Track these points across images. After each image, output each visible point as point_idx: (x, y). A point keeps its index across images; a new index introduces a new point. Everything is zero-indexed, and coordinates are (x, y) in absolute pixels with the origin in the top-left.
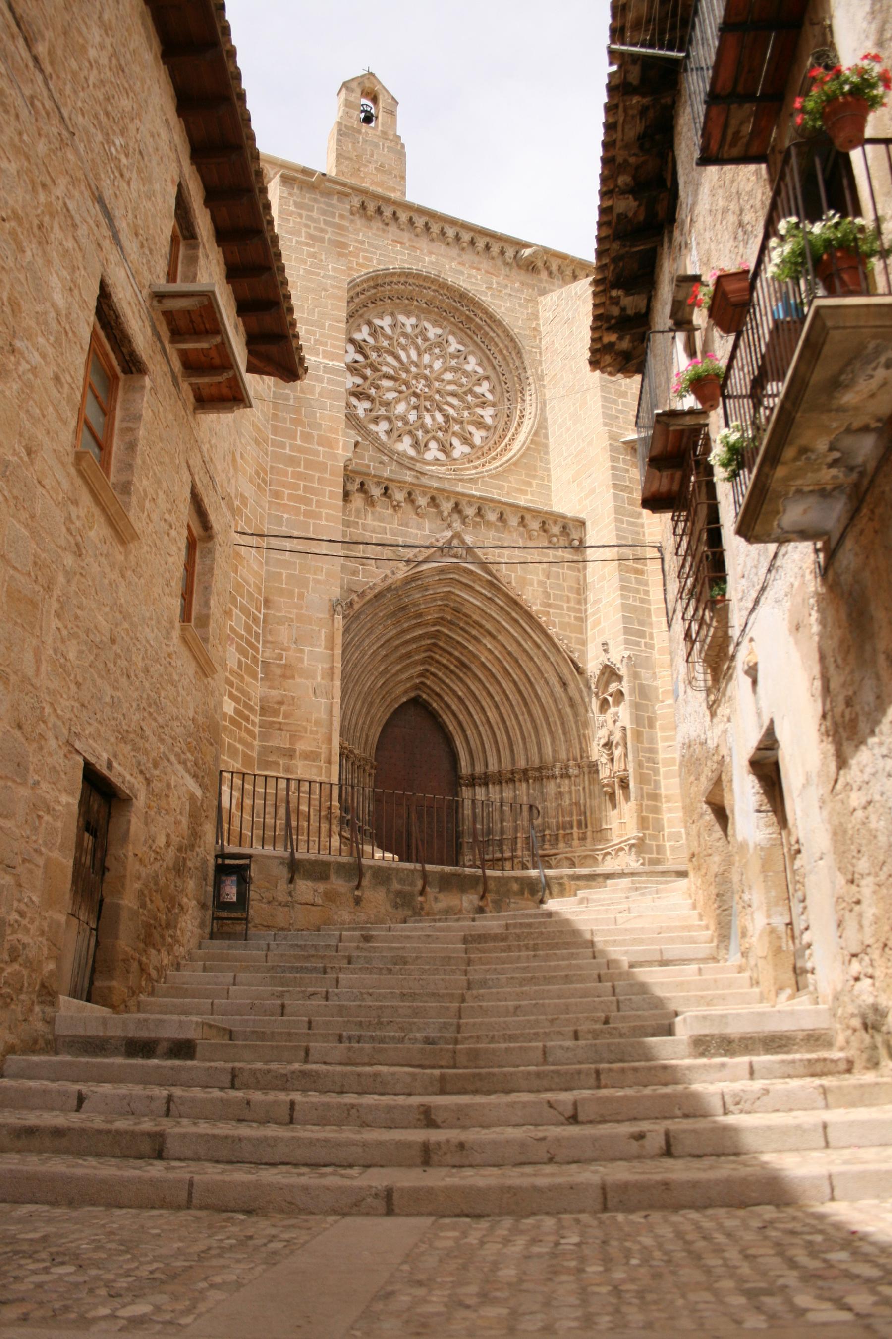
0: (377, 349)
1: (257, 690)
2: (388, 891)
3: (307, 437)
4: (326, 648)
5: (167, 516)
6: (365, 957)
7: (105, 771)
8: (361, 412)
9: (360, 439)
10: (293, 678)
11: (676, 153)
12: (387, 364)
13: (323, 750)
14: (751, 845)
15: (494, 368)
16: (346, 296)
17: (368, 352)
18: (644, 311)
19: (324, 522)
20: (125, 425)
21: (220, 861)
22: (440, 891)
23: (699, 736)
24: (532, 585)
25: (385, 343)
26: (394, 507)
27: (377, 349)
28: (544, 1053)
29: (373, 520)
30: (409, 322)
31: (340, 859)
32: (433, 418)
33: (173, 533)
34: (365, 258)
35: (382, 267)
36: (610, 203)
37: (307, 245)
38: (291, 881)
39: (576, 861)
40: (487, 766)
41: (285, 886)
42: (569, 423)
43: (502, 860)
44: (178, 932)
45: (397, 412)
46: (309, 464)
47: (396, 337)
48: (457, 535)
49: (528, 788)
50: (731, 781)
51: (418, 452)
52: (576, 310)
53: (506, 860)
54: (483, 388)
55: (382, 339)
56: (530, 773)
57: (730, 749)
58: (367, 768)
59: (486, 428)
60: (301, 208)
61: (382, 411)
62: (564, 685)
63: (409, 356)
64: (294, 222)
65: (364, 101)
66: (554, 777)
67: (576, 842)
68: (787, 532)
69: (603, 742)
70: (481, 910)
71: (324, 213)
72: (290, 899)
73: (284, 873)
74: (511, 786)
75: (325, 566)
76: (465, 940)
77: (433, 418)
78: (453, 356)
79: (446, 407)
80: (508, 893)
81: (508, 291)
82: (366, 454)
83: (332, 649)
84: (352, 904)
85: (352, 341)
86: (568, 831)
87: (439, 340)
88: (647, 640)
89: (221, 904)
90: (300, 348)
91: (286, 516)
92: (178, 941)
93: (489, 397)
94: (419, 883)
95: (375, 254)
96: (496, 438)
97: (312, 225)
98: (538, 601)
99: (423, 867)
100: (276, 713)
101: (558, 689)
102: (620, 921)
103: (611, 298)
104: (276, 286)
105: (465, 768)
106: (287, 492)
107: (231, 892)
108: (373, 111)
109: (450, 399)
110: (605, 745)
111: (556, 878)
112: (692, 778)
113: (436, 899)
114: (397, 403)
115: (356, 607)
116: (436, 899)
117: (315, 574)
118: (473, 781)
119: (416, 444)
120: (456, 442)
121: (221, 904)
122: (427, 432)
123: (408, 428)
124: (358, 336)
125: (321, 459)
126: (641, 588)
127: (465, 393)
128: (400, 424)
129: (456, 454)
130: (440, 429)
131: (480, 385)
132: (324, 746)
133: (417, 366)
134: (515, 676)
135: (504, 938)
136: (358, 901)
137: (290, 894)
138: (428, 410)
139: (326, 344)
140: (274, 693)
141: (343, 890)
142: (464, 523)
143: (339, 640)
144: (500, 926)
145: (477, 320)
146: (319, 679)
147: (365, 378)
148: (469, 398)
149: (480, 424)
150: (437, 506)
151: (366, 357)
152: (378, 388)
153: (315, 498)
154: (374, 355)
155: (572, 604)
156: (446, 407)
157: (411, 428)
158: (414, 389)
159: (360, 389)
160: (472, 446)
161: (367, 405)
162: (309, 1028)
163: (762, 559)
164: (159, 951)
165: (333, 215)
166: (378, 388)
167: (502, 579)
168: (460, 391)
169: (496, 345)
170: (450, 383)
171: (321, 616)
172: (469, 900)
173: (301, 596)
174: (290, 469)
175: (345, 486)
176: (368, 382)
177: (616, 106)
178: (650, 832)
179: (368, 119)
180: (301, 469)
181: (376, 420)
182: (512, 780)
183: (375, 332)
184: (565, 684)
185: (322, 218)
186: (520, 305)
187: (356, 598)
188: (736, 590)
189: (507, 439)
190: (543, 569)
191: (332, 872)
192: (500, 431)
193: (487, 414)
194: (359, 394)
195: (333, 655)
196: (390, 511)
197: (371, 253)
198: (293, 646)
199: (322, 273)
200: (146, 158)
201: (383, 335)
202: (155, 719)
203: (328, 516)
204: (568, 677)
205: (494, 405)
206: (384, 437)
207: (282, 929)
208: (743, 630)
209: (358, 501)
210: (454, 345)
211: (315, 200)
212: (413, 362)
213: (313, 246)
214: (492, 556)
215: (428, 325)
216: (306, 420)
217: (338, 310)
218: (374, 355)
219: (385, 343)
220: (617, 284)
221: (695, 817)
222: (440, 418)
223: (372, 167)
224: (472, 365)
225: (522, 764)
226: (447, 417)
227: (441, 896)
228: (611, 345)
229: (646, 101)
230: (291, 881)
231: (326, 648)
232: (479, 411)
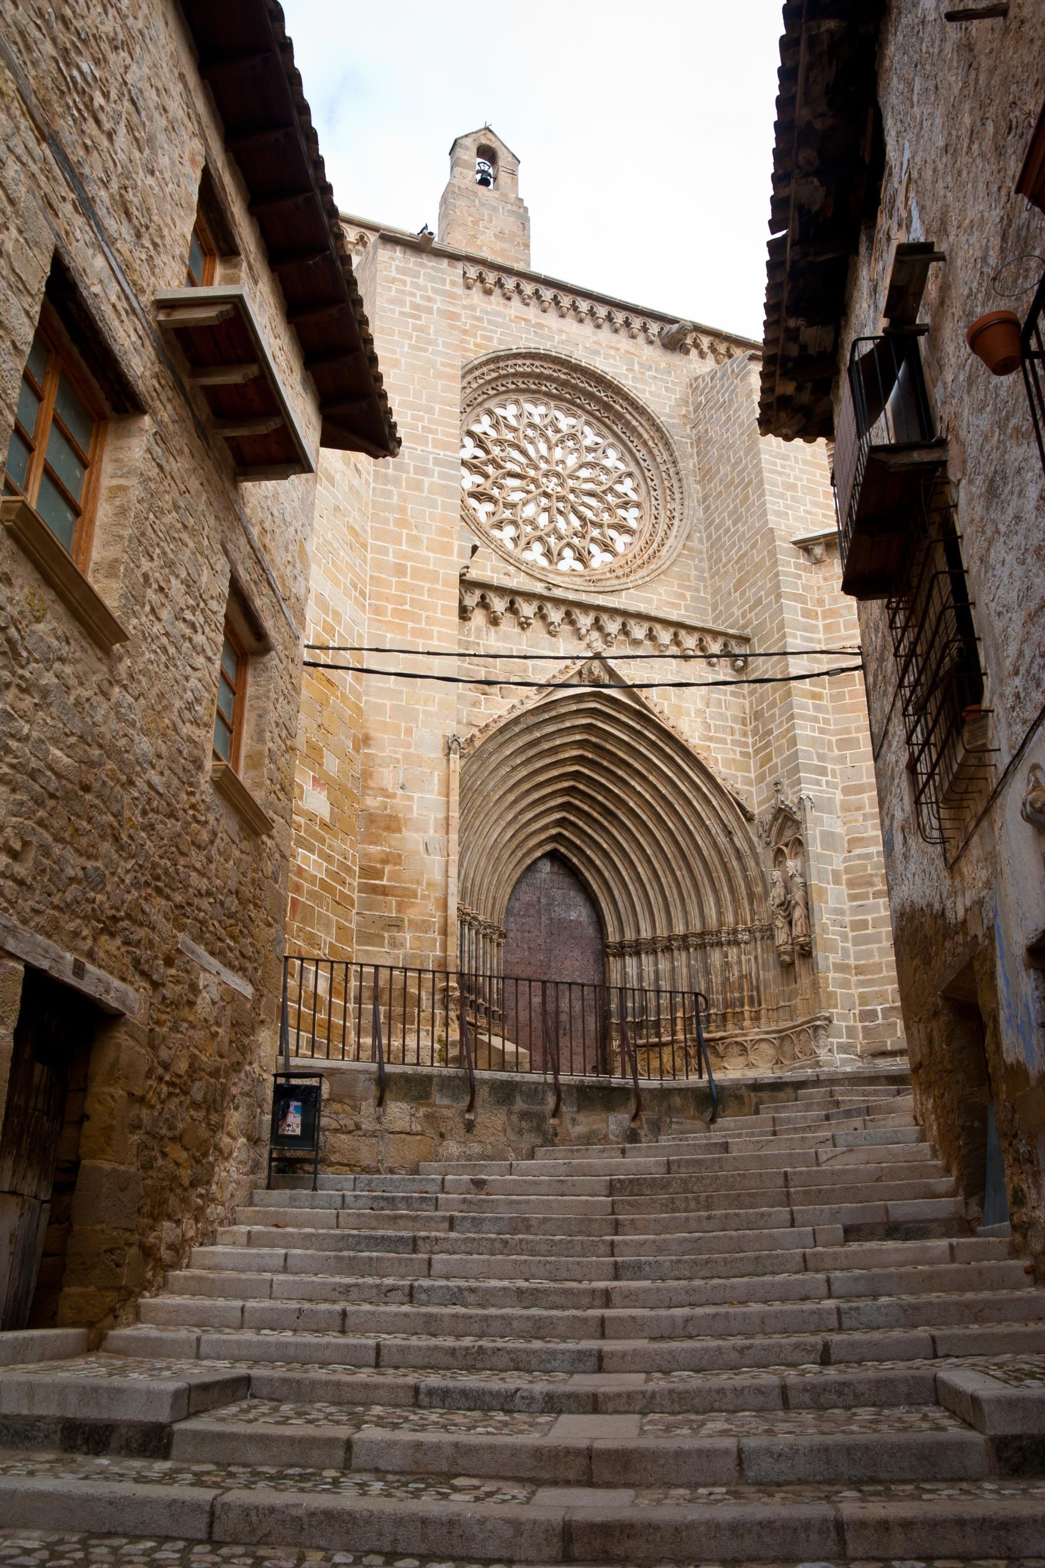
1: (351, 850)
2: (510, 1113)
3: (414, 541)
4: (439, 794)
5: (188, 615)
6: (473, 1219)
7: (70, 979)
8: (482, 517)
9: (478, 543)
10: (400, 831)
11: (881, 102)
12: (512, 460)
13: (437, 919)
15: (638, 463)
16: (460, 373)
17: (490, 445)
18: (829, 350)
20: (115, 482)
21: (281, 1081)
22: (579, 1110)
23: (930, 905)
24: (688, 714)
25: (510, 436)
26: (521, 624)
27: (499, 442)
28: (740, 1462)
29: (498, 640)
32: (568, 523)
34: (484, 337)
35: (503, 347)
37: (413, 316)
38: (380, 1102)
39: (748, 1046)
40: (638, 931)
41: (372, 1110)
42: (729, 523)
43: (661, 1045)
44: (214, 1187)
45: (524, 516)
46: (417, 573)
47: (522, 428)
49: (689, 959)
51: (551, 562)
52: (733, 391)
54: (627, 487)
55: (505, 431)
56: (692, 940)
57: (990, 928)
58: (495, 937)
59: (630, 532)
60: (405, 274)
61: (507, 514)
62: (729, 834)
63: (537, 451)
64: (397, 290)
67: (747, 1023)
69: (777, 902)
70: (633, 1137)
71: (432, 279)
72: (378, 1127)
73: (373, 1090)
74: (667, 955)
75: (438, 696)
76: (612, 1188)
77: (568, 523)
78: (589, 450)
79: (582, 509)
81: (652, 373)
82: (489, 564)
83: (448, 795)
84: (462, 1132)
85: (470, 434)
86: (738, 1010)
87: (573, 431)
88: (829, 778)
92: (213, 1200)
94: (551, 1100)
95: (495, 332)
96: (642, 543)
97: (418, 293)
98: (696, 734)
100: (379, 875)
101: (722, 839)
102: (823, 1157)
103: (787, 330)
105: (613, 937)
106: (390, 607)
107: (294, 1123)
110: (781, 905)
113: (574, 1121)
114: (524, 505)
115: (477, 744)
116: (574, 1120)
117: (426, 705)
118: (621, 951)
119: (548, 554)
121: (278, 1138)
122: (560, 538)
123: (538, 533)
124: (477, 429)
125: (431, 567)
126: (821, 716)
129: (595, 563)
130: (575, 534)
131: (621, 483)
132: (438, 914)
133: (547, 461)
134: (670, 824)
135: (665, 1186)
136: (470, 1126)
137: (378, 1119)
138: (560, 512)
139: (435, 432)
140: (374, 849)
142: (606, 642)
143: (455, 785)
145: (617, 407)
146: (431, 831)
147: (486, 476)
148: (610, 498)
149: (622, 528)
150: (572, 623)
151: (487, 452)
152: (501, 487)
153: (424, 614)
154: (496, 451)
155: (737, 737)
156: (582, 509)
157: (542, 533)
158: (544, 488)
159: (480, 489)
160: (615, 554)
161: (489, 507)
162: (430, 1259)
164: (178, 1222)
165: (443, 281)
166: (501, 487)
168: (599, 489)
169: (640, 436)
170: (586, 480)
171: (433, 755)
172: (616, 1121)
173: (409, 731)
174: (394, 580)
175: (461, 602)
176: (490, 481)
178: (839, 1010)
179: (484, 182)
180: (408, 580)
181: (499, 525)
182: (668, 949)
184: (730, 833)
185: (429, 285)
186: (667, 389)
187: (478, 734)
189: (655, 545)
190: (702, 696)
191: (434, 1089)
192: (646, 535)
193: (631, 516)
194: (479, 496)
195: (448, 802)
196: (517, 630)
197: (491, 331)
198: (400, 792)
199: (430, 348)
200: (143, 114)
201: (507, 426)
202: (168, 898)
205: (638, 505)
206: (510, 545)
207: (366, 1170)
209: (479, 618)
210: (590, 437)
211: (422, 265)
212: (542, 457)
213: (419, 318)
215: (559, 415)
216: (412, 521)
217: (451, 393)
218: (496, 451)
220: (794, 311)
222: (576, 522)
223: (490, 234)
224: (612, 459)
225: (680, 929)
227: (581, 1118)
230: (380, 1102)
231: (439, 794)
232: (621, 512)
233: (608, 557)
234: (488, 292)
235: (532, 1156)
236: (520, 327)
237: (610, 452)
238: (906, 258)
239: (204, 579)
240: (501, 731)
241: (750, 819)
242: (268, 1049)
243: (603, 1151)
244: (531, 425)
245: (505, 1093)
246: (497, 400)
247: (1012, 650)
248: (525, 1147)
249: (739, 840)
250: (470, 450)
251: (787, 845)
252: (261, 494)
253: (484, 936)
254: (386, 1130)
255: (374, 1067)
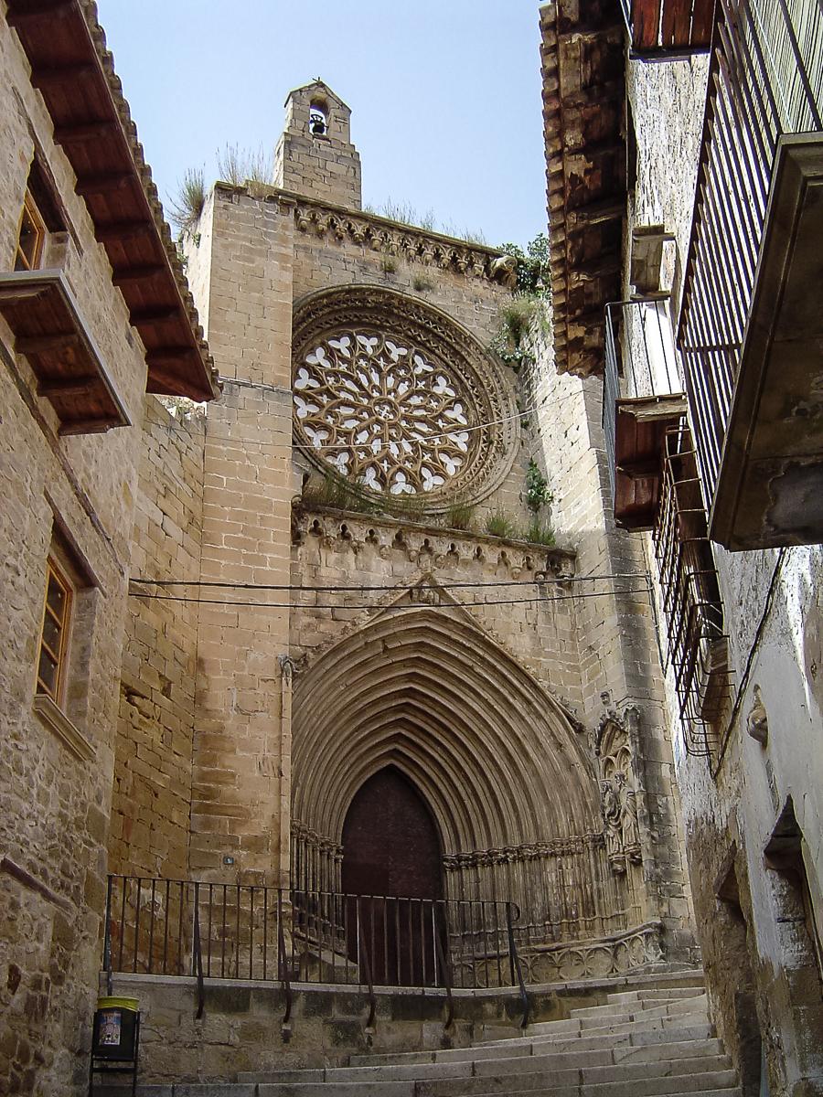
0: (335, 374)
8: (317, 444)
10: (233, 751)
14: (776, 967)
19: (268, 568)
25: (343, 367)
27: (335, 374)
30: (369, 343)
31: (263, 985)
33: (21, 581)
36: (559, 167)
38: (199, 1015)
48: (428, 577)
50: (745, 875)
53: (502, 957)
59: (460, 455)
63: (370, 381)
65: (313, 111)
66: (554, 855)
68: (784, 531)
73: (190, 1005)
77: (399, 447)
80: (481, 1017)
89: (99, 1050)
90: (211, 361)
91: (223, 562)
93: (463, 422)
99: (370, 989)
102: (618, 1056)
104: (172, 286)
108: (324, 121)
109: (418, 425)
111: (542, 995)
112: (702, 866)
120: (426, 473)
122: (392, 462)
127: (436, 418)
128: (362, 455)
129: (427, 486)
130: (407, 459)
131: (452, 409)
136: (286, 1037)
141: (265, 1024)
144: (464, 1067)
147: (320, 406)
149: (452, 452)
152: (336, 416)
156: (414, 435)
159: (314, 419)
160: (445, 476)
161: (324, 436)
163: (761, 577)
166: (336, 416)
167: (481, 625)
172: (430, 1030)
175: (293, 528)
177: (554, 49)
181: (334, 453)
183: (331, 354)
188: (734, 623)
194: (316, 425)
203: (275, 558)
204: (564, 738)
208: (746, 676)
209: (311, 543)
210: (421, 366)
214: (466, 595)
215: (390, 345)
219: (343, 367)
221: (709, 916)
222: (407, 448)
224: (442, 387)
226: (414, 444)
227: (395, 1026)
228: (579, 341)
229: (588, 38)
230: (199, 1015)
232: (451, 437)
233: (439, 481)
234: (320, 234)
235: (347, 1063)
236: (343, 267)
237: (441, 380)
238: (641, 239)
239: (27, 525)
240: (335, 651)
241: (580, 729)
242: (91, 964)
243: (416, 1056)
244: (364, 356)
245: (320, 1004)
246: (330, 334)
247: (737, 584)
248: (341, 1055)
249: (571, 751)
250: (305, 381)
251: (615, 756)
252: (83, 444)
253: (321, 852)
254: (206, 1042)
255: (194, 980)
